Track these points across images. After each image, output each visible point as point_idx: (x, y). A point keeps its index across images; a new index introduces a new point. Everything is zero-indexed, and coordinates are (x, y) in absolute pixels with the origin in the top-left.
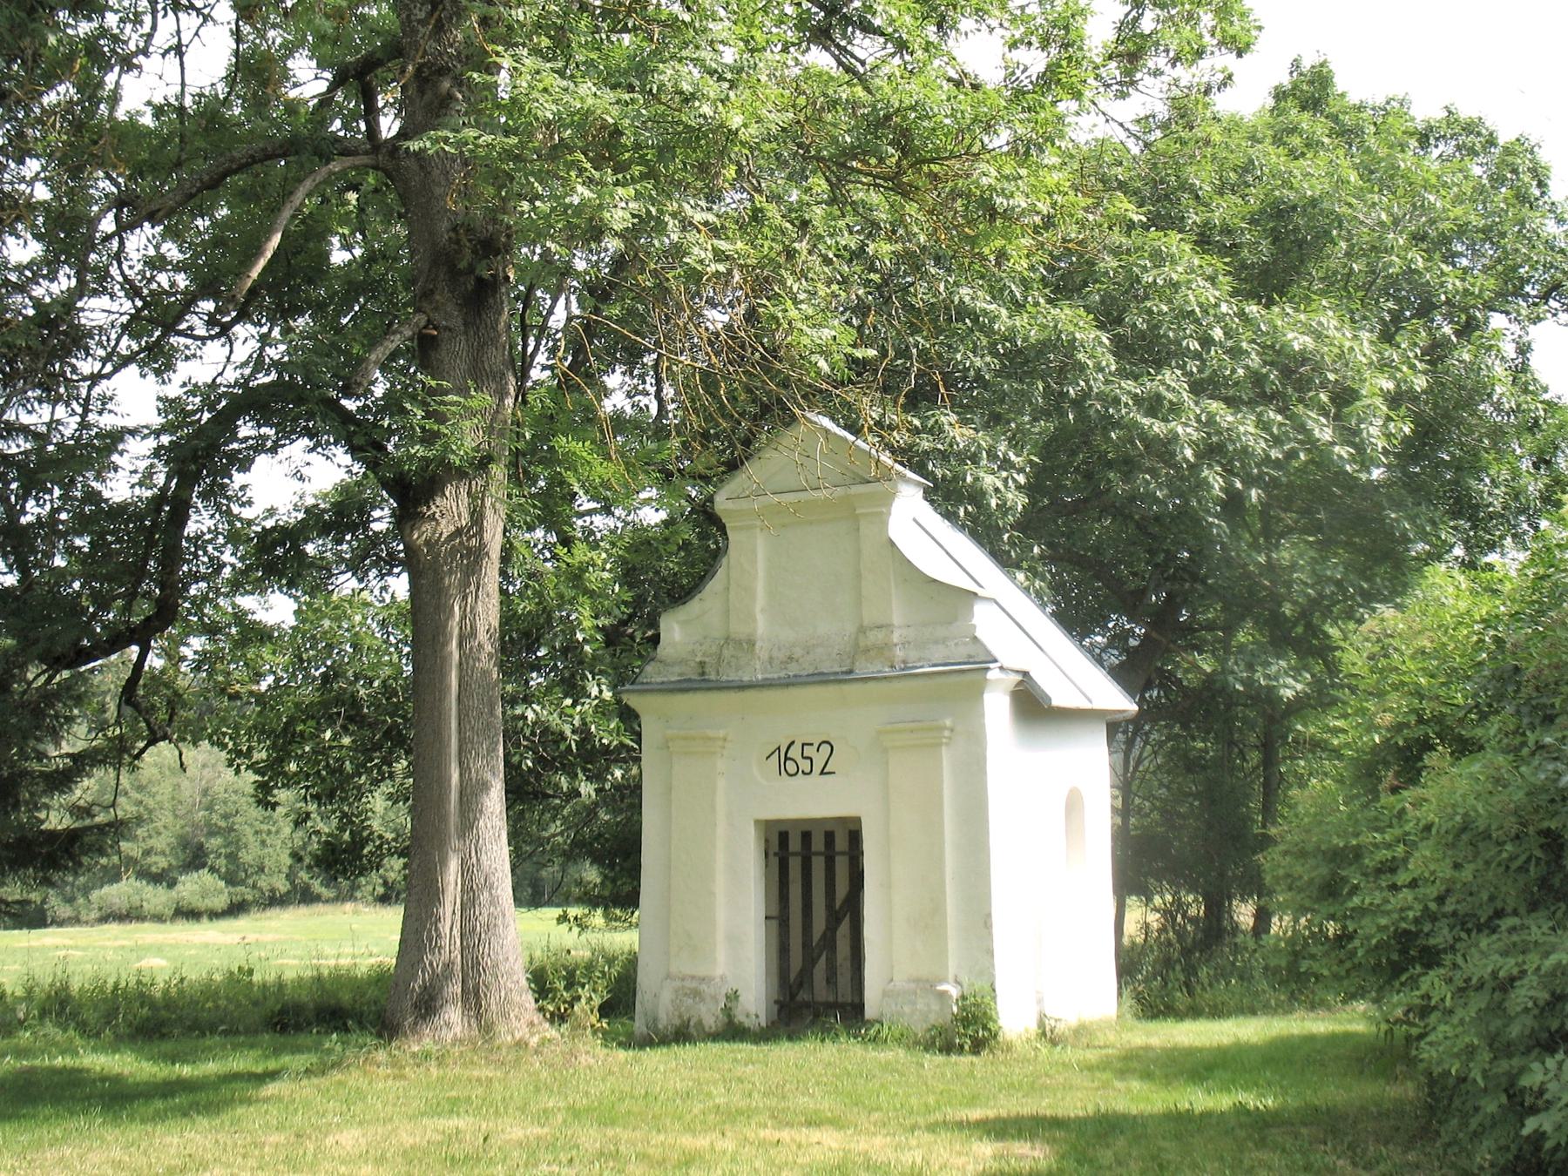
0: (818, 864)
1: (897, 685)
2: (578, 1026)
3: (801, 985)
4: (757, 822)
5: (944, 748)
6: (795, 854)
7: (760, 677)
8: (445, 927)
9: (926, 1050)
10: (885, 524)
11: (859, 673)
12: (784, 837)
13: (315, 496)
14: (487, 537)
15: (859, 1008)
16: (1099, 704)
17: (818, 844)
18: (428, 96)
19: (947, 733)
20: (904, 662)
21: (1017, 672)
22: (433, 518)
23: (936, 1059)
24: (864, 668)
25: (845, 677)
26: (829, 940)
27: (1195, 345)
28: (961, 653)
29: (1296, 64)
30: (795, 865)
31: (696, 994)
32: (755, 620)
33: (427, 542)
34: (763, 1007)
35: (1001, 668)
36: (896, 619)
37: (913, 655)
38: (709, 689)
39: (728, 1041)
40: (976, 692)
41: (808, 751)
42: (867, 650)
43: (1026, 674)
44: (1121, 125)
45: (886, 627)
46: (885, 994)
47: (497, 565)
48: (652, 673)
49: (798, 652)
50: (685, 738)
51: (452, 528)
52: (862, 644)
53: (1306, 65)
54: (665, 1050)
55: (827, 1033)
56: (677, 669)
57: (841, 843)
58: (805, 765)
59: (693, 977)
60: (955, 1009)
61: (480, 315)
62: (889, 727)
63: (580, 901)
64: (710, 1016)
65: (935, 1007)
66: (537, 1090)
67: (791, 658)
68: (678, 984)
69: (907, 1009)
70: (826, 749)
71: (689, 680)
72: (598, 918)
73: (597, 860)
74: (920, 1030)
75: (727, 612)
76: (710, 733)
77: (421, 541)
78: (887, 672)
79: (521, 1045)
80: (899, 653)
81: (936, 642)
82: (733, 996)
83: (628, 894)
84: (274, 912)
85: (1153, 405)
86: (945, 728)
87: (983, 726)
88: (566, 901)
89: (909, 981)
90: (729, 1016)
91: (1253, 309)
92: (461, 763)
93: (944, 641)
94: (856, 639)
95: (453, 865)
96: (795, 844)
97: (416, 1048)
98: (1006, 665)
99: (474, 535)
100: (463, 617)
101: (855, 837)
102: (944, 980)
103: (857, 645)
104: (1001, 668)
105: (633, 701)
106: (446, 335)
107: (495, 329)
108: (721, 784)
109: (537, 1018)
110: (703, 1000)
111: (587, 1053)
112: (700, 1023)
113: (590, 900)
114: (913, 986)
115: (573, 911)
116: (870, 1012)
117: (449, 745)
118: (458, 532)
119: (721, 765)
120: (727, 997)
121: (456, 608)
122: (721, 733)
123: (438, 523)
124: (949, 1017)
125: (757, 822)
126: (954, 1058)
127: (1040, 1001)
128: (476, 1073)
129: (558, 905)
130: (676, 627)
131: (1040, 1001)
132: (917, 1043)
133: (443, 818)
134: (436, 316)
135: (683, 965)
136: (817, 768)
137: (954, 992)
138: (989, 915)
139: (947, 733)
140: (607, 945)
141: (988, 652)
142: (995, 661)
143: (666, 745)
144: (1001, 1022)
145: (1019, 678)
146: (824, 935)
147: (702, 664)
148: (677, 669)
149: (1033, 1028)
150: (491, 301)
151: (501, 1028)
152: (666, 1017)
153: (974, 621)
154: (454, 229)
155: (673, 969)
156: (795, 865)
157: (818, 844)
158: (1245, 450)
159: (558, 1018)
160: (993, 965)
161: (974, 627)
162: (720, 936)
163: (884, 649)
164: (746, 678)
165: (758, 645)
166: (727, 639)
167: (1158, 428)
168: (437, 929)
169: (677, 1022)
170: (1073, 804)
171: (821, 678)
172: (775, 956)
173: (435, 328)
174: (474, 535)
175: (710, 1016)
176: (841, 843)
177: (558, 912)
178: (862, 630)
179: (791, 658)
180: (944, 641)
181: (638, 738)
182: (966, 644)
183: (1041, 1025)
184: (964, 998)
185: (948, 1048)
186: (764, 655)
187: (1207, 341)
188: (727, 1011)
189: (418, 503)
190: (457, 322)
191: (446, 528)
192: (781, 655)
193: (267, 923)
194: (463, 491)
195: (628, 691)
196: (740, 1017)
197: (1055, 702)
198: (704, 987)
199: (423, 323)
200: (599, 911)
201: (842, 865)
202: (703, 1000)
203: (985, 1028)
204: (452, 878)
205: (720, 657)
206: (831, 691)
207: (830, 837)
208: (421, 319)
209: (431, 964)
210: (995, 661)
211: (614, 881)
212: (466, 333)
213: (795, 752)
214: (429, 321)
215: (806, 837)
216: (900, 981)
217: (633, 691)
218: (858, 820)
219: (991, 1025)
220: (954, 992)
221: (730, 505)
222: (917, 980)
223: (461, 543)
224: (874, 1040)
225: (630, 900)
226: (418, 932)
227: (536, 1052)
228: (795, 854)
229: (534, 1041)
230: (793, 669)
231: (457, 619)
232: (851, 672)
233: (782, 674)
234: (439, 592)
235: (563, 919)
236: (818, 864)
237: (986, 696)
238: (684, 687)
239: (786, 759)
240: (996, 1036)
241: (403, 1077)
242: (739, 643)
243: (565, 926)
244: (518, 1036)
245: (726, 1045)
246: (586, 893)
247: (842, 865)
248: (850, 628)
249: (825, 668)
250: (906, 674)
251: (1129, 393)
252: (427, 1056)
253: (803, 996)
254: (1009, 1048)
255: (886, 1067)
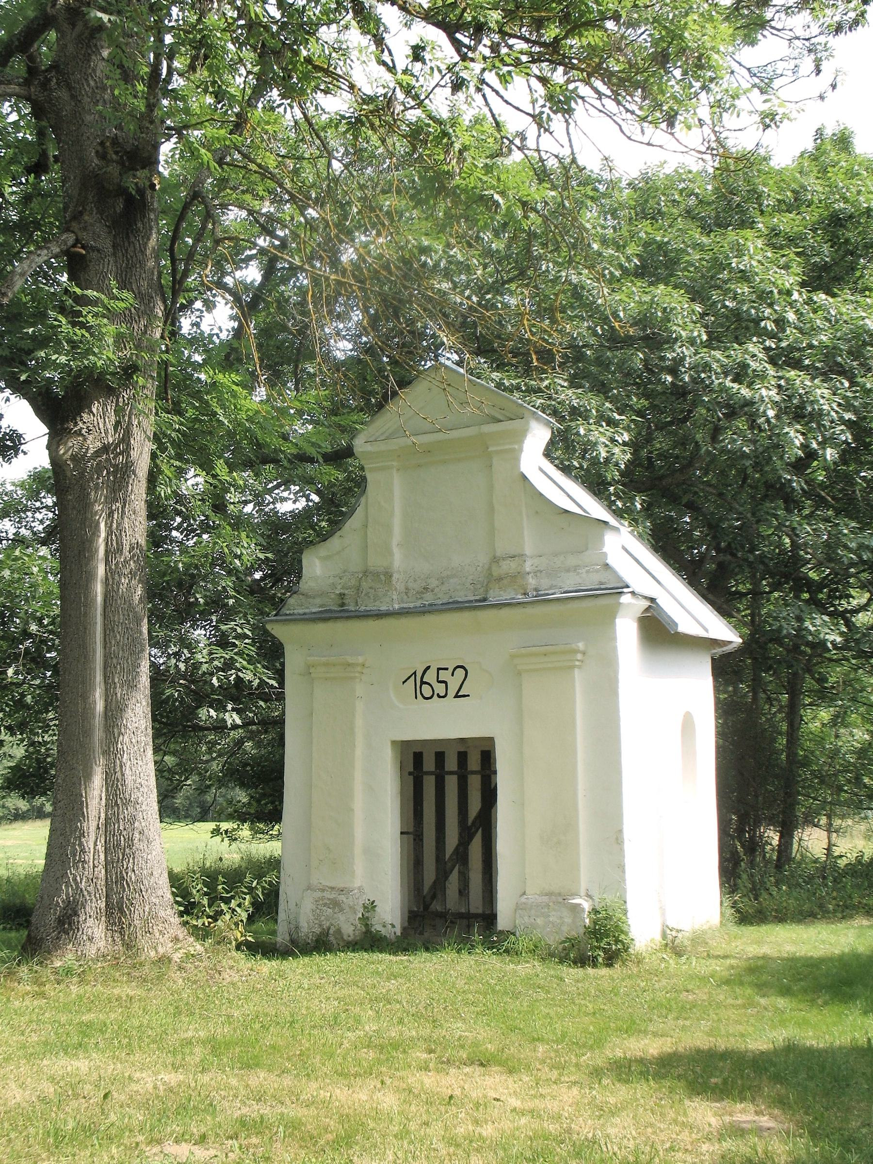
0: (451, 784)
1: (529, 610)
2: (222, 941)
3: (434, 897)
4: (394, 743)
5: (576, 671)
6: (429, 773)
7: (396, 606)
8: (89, 843)
9: (561, 962)
10: (516, 460)
11: (492, 600)
12: (418, 758)
13: (13, 484)
14: (134, 454)
15: (489, 919)
16: (713, 635)
17: (451, 764)
18: (80, 26)
19: (579, 656)
20: (536, 590)
21: (646, 598)
22: (79, 433)
23: (571, 974)
24: (496, 595)
25: (481, 604)
26: (462, 855)
27: (770, 326)
28: (591, 580)
29: (819, 133)
30: (429, 783)
31: (335, 904)
32: (391, 553)
33: (74, 458)
34: (398, 913)
35: (633, 593)
36: (528, 551)
37: (545, 583)
38: (348, 618)
39: (366, 950)
40: (610, 616)
41: (443, 675)
42: (500, 579)
43: (653, 600)
44: (749, 69)
45: (519, 557)
46: (518, 907)
47: (144, 484)
48: (294, 606)
49: (433, 583)
50: (326, 665)
51: (99, 444)
52: (495, 574)
53: (828, 132)
54: (307, 959)
55: (464, 944)
56: (318, 601)
57: (474, 763)
58: (440, 689)
59: (333, 888)
60: (587, 921)
61: (128, 237)
62: (523, 651)
63: (230, 818)
64: (349, 927)
65: (568, 920)
66: (178, 1012)
67: (426, 589)
68: (319, 894)
69: (539, 921)
70: (460, 673)
71: (330, 611)
72: (245, 832)
73: (243, 785)
74: (553, 940)
75: (365, 548)
76: (350, 659)
77: (67, 456)
78: (520, 598)
79: (164, 960)
80: (532, 581)
81: (568, 570)
82: (370, 907)
83: (270, 812)
84: (18, 825)
85: (741, 374)
86: (577, 651)
87: (615, 649)
88: (219, 817)
89: (542, 894)
90: (367, 925)
91: (821, 297)
92: (106, 677)
93: (576, 569)
94: (490, 569)
95: (98, 780)
96: (429, 764)
97: (58, 964)
98: (637, 590)
99: (121, 453)
100: (110, 533)
101: (487, 757)
102: (576, 894)
103: (491, 574)
104: (633, 593)
105: (278, 630)
106: (94, 255)
107: (143, 252)
108: (360, 706)
109: (181, 933)
110: (341, 910)
111: (231, 968)
112: (339, 931)
113: (241, 817)
114: (545, 899)
115: (225, 826)
116: (503, 922)
117: (94, 661)
118: (105, 449)
119: (360, 689)
120: (365, 907)
121: (102, 526)
122: (360, 659)
123: (85, 439)
124: (582, 931)
125: (394, 743)
126: (590, 971)
127: (663, 914)
128: (116, 991)
129: (213, 820)
130: (317, 562)
131: (663, 914)
132: (552, 955)
133: (88, 733)
134: (84, 236)
135: (323, 877)
136: (452, 692)
137: (586, 905)
138: (621, 831)
139: (579, 656)
140: (254, 852)
141: (619, 578)
142: (628, 587)
143: (307, 672)
144: (631, 935)
145: (647, 604)
146: (457, 848)
147: (342, 596)
148: (318, 601)
149: (658, 937)
150: (140, 225)
151: (143, 942)
152: (307, 927)
153: (605, 550)
154: (102, 144)
155: (314, 882)
156: (429, 783)
157: (451, 764)
158: (821, 412)
159: (201, 934)
160: (624, 880)
161: (605, 554)
162: (358, 850)
163: (517, 577)
164: (384, 608)
165: (396, 576)
166: (365, 573)
167: (745, 392)
168: (81, 844)
169: (318, 930)
170: (688, 725)
171: (455, 606)
172: (412, 867)
173: (83, 247)
174: (121, 453)
175: (349, 927)
176: (474, 763)
177: (212, 825)
178: (495, 560)
179: (426, 589)
180: (576, 569)
181: (280, 675)
182: (597, 571)
183: (664, 936)
184: (595, 911)
185: (582, 961)
186: (401, 587)
187: (781, 322)
188: (364, 920)
189: (65, 420)
190: (105, 243)
191: (93, 445)
192: (417, 586)
193: (11, 833)
194: (111, 409)
195: (271, 621)
196: (377, 927)
197: (682, 629)
198: (342, 898)
199: (71, 242)
200: (246, 825)
201: (475, 783)
202: (341, 910)
203: (617, 941)
204: (96, 793)
205: (358, 589)
206: (467, 615)
207: (462, 757)
208: (70, 238)
209: (75, 880)
210: (628, 587)
211: (258, 801)
212: (114, 254)
213: (430, 677)
214: (77, 241)
215: (440, 757)
216: (533, 895)
217: (276, 621)
218: (491, 740)
219: (622, 937)
220: (586, 905)
221: (369, 448)
222: (550, 894)
223: (108, 460)
224: (507, 951)
225: (275, 816)
226: (63, 847)
227: (180, 968)
228: (429, 773)
229: (177, 957)
230: (429, 598)
231: (103, 535)
232: (485, 600)
233: (418, 604)
234: (85, 505)
235: (216, 832)
236: (451, 784)
237: (618, 621)
238: (324, 617)
239: (422, 683)
240: (626, 950)
241: (43, 995)
242: (376, 575)
243: (218, 839)
244: (161, 950)
245: (366, 955)
246: (235, 811)
247: (475, 783)
248: (483, 559)
249: (461, 596)
250: (541, 600)
251: (718, 361)
252: (69, 972)
253: (436, 906)
254: (639, 962)
255: (528, 981)
